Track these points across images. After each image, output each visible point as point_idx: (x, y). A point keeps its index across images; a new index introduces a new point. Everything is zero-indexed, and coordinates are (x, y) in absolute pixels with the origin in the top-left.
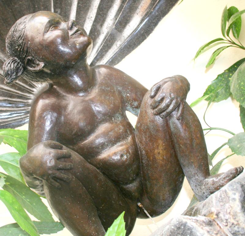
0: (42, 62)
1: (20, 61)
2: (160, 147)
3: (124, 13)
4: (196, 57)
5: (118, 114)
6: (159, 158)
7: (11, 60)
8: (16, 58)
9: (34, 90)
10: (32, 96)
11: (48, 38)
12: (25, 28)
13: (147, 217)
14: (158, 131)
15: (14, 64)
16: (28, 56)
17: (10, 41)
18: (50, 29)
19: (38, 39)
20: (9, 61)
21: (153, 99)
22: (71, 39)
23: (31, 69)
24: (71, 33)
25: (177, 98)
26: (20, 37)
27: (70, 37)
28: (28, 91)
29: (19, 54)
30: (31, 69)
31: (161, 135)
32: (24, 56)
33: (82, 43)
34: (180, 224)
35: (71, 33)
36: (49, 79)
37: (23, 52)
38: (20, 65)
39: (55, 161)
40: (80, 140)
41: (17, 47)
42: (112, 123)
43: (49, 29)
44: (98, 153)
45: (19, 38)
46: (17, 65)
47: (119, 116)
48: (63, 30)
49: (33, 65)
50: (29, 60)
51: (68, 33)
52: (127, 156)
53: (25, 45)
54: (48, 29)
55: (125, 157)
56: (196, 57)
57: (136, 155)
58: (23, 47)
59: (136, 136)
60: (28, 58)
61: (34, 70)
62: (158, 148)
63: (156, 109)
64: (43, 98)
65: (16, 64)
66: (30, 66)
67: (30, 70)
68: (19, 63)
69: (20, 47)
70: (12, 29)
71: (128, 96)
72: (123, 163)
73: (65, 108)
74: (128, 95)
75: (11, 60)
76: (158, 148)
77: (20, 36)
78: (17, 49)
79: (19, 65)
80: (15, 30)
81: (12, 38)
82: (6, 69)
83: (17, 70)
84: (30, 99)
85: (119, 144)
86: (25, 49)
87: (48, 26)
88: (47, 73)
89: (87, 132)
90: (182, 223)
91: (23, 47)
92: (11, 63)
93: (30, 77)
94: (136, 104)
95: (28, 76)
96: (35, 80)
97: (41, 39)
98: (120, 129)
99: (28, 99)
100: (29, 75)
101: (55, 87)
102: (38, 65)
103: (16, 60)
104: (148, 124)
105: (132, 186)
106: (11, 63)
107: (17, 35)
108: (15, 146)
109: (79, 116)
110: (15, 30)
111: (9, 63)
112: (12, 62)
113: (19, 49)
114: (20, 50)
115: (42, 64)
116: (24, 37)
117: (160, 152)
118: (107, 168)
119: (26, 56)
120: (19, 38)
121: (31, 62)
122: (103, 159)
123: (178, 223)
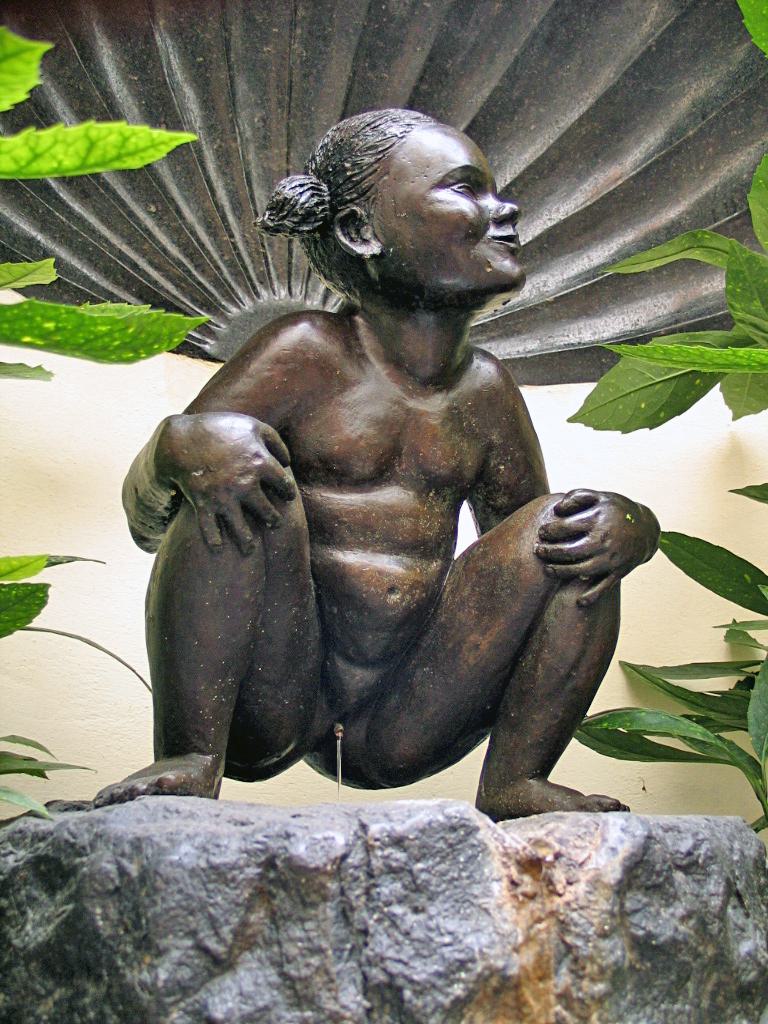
0: (380, 244)
1: (329, 202)
2: (491, 635)
3: (111, 262)
4: (731, 491)
5: (449, 492)
6: (470, 658)
7: (311, 183)
8: (324, 187)
9: (264, 293)
10: (248, 305)
11: (440, 201)
12: (402, 138)
13: (336, 780)
14: (514, 593)
15: (312, 196)
16: (357, 205)
17: (342, 140)
18: (455, 187)
19: (417, 185)
20: (307, 181)
21: (558, 519)
22: (485, 245)
23: (342, 239)
24: (493, 231)
25: (613, 556)
26: (374, 147)
27: (485, 238)
28: (247, 287)
29: (341, 184)
30: (342, 239)
31: (516, 608)
32: (348, 198)
33: (497, 273)
34: (463, 822)
36: (358, 294)
37: (354, 187)
38: (323, 210)
39: (255, 483)
40: (323, 483)
41: (347, 165)
42: (423, 503)
43: (454, 184)
44: (343, 545)
45: (369, 148)
46: (317, 204)
47: (448, 498)
48: (481, 210)
49: (353, 232)
50: (354, 213)
51: (487, 228)
52: (402, 600)
53: (370, 174)
54: (451, 181)
55: (395, 598)
56: (731, 491)
57: (422, 614)
58: (364, 174)
59: (451, 573)
60: (354, 208)
61: (346, 246)
62: (483, 634)
63: (549, 547)
64: (313, 325)
65: (316, 200)
66: (342, 230)
67: (336, 239)
68: (322, 203)
69: (357, 171)
70: (368, 117)
71: (500, 470)
72: (385, 606)
73: (346, 384)
74: (502, 467)
75: (311, 183)
76: (483, 634)
77: (376, 147)
78: (346, 170)
79: (321, 208)
80: (373, 125)
81: (353, 137)
82: (286, 191)
83: (309, 215)
84: (239, 307)
85: (407, 560)
86: (364, 185)
87: (458, 175)
88: (367, 274)
89: (355, 477)
90: (467, 823)
91: (364, 174)
92: (306, 188)
93: (320, 254)
94: (502, 500)
95: (316, 248)
96: (327, 271)
97: (422, 190)
98: (429, 529)
99: (234, 300)
100: (321, 251)
101: (359, 320)
102: (365, 241)
103: (321, 190)
104: (505, 565)
105: (358, 678)
106: (306, 188)
107: (372, 138)
109: (368, 427)
110: (373, 125)
111: (301, 186)
112: (312, 188)
113: (348, 174)
114: (352, 176)
115: (374, 248)
116: (384, 156)
117: (479, 644)
118: (333, 586)
119: (352, 201)
120: (369, 148)
121: (352, 223)
122: (345, 565)
123: (458, 815)
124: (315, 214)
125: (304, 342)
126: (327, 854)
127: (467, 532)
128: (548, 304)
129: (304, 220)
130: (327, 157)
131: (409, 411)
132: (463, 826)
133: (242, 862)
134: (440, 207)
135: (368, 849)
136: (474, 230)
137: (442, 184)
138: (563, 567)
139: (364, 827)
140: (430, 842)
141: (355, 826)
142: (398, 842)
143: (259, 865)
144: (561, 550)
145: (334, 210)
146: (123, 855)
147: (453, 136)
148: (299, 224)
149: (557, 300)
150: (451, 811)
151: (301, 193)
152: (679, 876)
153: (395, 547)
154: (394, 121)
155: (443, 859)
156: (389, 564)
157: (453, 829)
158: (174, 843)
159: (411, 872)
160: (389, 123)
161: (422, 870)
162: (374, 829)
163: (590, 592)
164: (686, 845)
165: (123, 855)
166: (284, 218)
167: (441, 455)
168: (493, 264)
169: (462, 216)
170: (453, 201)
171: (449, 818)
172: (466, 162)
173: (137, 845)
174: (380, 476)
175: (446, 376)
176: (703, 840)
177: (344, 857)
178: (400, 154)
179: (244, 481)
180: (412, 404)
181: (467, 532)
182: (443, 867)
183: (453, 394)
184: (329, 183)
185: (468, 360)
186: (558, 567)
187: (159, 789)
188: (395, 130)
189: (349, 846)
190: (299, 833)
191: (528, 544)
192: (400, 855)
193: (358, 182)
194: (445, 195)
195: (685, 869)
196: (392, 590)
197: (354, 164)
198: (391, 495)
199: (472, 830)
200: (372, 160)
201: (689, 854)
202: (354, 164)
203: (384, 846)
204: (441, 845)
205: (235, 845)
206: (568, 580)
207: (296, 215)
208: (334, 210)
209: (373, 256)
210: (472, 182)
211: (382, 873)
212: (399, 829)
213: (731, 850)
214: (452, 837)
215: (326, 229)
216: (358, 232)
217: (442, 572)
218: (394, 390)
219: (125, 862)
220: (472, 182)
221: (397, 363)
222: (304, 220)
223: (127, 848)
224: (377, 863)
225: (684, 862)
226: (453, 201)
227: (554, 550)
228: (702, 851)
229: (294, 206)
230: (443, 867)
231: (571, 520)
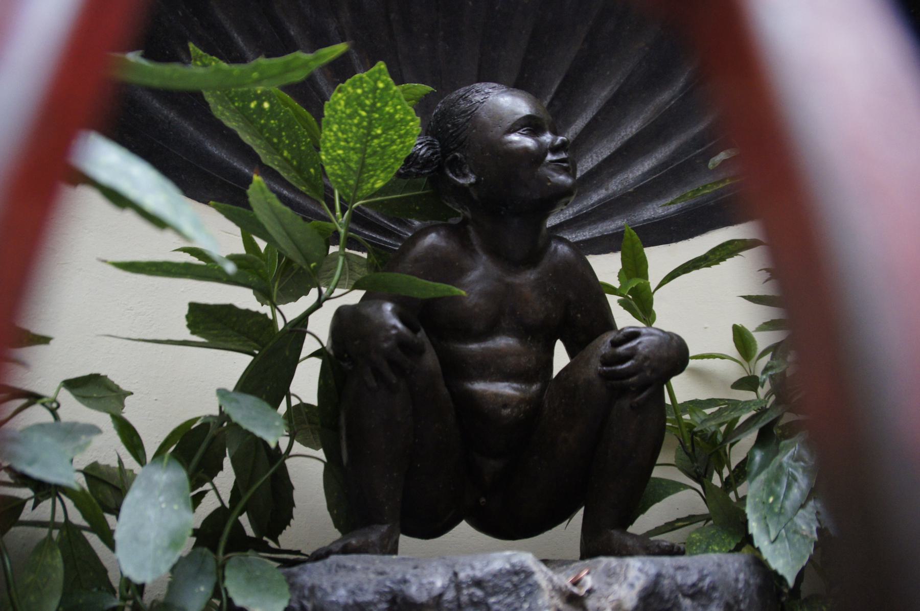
15: (428, 149)
23: (451, 175)
24: (550, 157)
30: (451, 175)
35: (550, 157)
46: (432, 154)
51: (546, 155)
64: (438, 234)
65: (431, 152)
78: (449, 129)
101: (470, 228)
102: (465, 176)
107: (463, 105)
108: (335, 512)
115: (472, 179)
116: (471, 115)
118: (471, 406)
121: (457, 166)
124: (431, 161)
125: (433, 247)
126: (429, 593)
127: (561, 358)
128: (630, 194)
129: (424, 166)
130: (438, 122)
131: (508, 285)
132: (524, 571)
133: (375, 601)
134: (515, 146)
135: (458, 586)
136: (535, 158)
137: (512, 130)
138: (618, 382)
139: (456, 574)
140: (500, 583)
141: (450, 574)
142: (478, 583)
143: (387, 602)
144: (615, 371)
145: (444, 156)
146: (304, 597)
147: (519, 96)
148: (422, 169)
149: (636, 190)
150: (515, 560)
151: (420, 149)
152: (686, 603)
153: (506, 377)
154: (477, 92)
155: (510, 595)
156: (505, 389)
157: (516, 573)
158: (334, 588)
159: (487, 605)
160: (475, 94)
161: (494, 603)
162: (462, 576)
163: (638, 398)
164: (693, 578)
165: (304, 597)
166: (410, 167)
167: (537, 307)
168: (552, 179)
169: (526, 150)
170: (521, 140)
171: (513, 565)
172: (528, 113)
173: (312, 589)
174: (491, 331)
175: (533, 257)
176: (707, 575)
177: (441, 595)
178: (483, 114)
179: (386, 345)
180: (510, 279)
181: (561, 358)
182: (509, 600)
183: (539, 269)
184: (439, 139)
185: (548, 245)
186: (614, 382)
187: (346, 550)
188: (478, 98)
189: (445, 589)
190: (413, 580)
191: (595, 366)
192: (479, 593)
193: (457, 136)
194: (515, 137)
195: (692, 597)
196: (505, 406)
197: (454, 125)
198: (503, 342)
199: (529, 574)
200: (465, 120)
201: (694, 585)
202: (454, 125)
203: (469, 586)
204: (508, 585)
205: (371, 588)
206: (624, 391)
207: (418, 163)
208: (444, 156)
209: (471, 184)
210: (531, 125)
211: (467, 605)
212: (479, 574)
213: (737, 580)
214: (515, 579)
215: (440, 169)
216: (460, 169)
217: (542, 391)
218: (495, 271)
219: (305, 603)
220: (531, 125)
221: (497, 253)
222: (424, 166)
223: (306, 592)
224: (464, 599)
225: (691, 592)
226: (521, 140)
227: (610, 371)
228: (708, 580)
229: (416, 158)
230: (509, 600)
231: (621, 349)
